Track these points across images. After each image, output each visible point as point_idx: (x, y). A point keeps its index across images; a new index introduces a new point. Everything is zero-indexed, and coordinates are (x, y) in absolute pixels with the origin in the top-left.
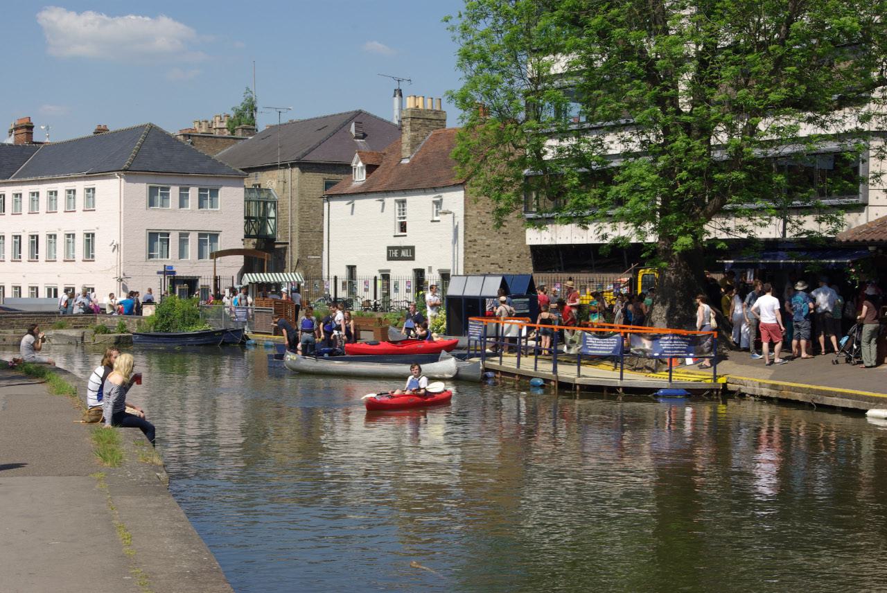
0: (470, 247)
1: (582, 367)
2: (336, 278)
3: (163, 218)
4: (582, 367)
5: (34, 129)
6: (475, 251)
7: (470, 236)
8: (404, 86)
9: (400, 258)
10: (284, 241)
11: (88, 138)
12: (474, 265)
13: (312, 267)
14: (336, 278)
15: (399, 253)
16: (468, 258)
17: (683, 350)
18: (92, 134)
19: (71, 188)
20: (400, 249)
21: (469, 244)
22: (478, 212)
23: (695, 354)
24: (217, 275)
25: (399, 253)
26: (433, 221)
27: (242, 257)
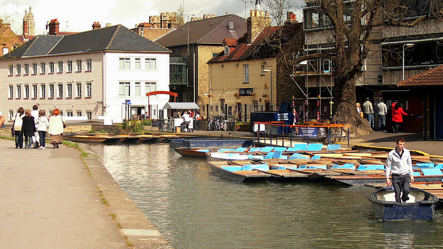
0: (280, 89)
1: (266, 140)
2: (246, 105)
3: (15, 81)
4: (266, 140)
5: (59, 25)
6: (282, 90)
7: (280, 83)
8: (15, 13)
9: (246, 95)
10: (92, 92)
11: (127, 29)
12: (282, 98)
13: (206, 99)
14: (246, 105)
15: (245, 92)
16: (279, 94)
17: (311, 133)
18: (91, 29)
19: (26, 63)
20: (246, 90)
21: (279, 87)
22: (284, 71)
23: (317, 135)
24: (150, 104)
25: (245, 92)
26: (11, 87)
27: (169, 95)
